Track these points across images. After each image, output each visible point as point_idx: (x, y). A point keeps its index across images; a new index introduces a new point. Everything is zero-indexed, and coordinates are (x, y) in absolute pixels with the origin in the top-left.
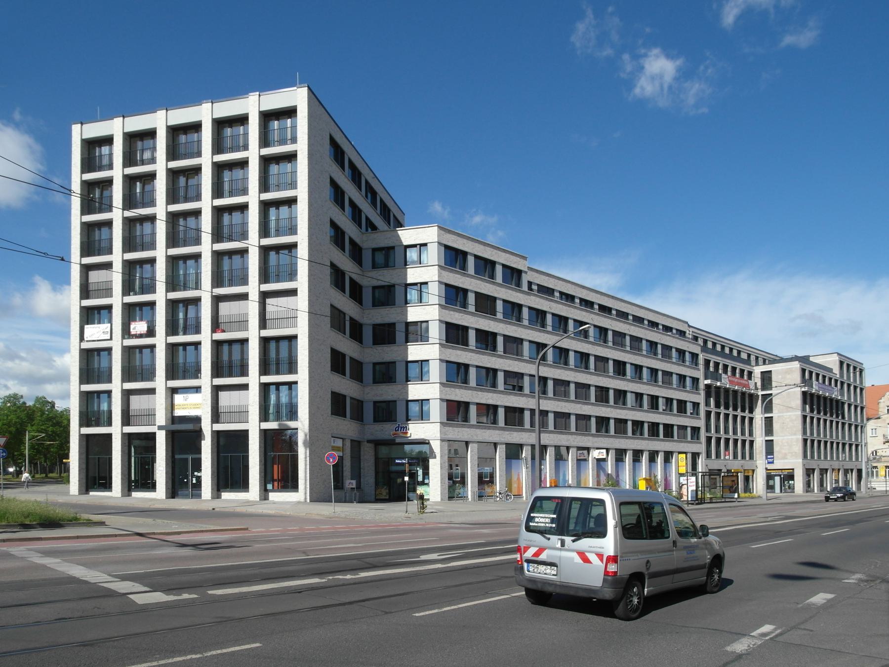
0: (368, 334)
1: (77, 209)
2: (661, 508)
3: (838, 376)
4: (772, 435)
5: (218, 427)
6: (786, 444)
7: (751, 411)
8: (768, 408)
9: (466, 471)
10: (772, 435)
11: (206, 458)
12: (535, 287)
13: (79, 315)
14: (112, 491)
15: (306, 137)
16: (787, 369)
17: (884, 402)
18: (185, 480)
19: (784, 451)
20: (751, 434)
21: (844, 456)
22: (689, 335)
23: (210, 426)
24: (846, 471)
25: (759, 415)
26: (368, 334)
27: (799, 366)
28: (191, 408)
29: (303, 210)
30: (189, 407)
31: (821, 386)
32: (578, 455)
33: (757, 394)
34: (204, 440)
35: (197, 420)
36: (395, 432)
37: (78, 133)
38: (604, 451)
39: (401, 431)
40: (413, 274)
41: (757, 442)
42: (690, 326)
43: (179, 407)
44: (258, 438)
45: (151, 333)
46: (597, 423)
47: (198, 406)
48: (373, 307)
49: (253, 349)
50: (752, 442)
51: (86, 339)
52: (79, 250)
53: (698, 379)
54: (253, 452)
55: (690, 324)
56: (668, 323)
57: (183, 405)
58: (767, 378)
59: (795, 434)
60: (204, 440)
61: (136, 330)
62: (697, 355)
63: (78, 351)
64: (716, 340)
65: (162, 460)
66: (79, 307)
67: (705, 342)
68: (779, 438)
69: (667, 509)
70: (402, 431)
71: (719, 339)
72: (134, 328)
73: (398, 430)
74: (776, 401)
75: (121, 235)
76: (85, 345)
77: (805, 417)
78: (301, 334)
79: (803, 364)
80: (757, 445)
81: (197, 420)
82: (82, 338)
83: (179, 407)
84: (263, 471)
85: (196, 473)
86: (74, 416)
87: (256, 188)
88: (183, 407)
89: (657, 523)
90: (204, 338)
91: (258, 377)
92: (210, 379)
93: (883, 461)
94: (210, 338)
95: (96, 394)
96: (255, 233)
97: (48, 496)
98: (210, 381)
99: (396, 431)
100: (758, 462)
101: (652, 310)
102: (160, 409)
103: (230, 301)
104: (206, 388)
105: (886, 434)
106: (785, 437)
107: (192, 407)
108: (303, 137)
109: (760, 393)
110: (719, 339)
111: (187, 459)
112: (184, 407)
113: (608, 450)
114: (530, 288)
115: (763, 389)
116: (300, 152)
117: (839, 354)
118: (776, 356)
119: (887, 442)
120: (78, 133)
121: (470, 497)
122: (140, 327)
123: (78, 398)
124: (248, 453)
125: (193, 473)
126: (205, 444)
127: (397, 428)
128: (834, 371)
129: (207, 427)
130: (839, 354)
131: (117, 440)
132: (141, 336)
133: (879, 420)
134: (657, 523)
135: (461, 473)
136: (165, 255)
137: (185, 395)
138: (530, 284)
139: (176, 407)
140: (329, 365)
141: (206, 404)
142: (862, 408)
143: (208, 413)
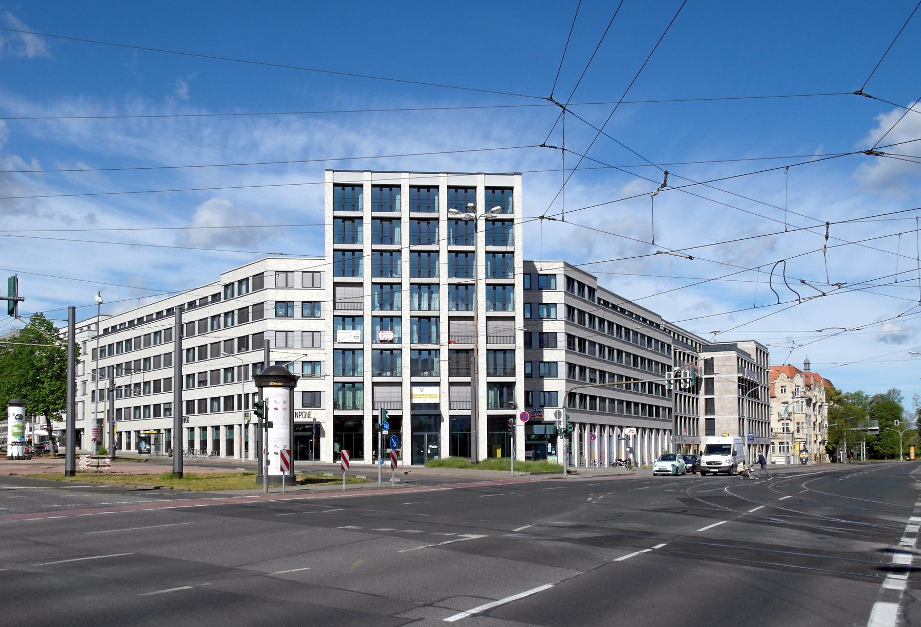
1: (330, 239)
3: (755, 361)
4: (713, 414)
5: (453, 413)
6: (725, 423)
7: (697, 394)
8: (710, 388)
10: (713, 414)
12: (602, 302)
14: (364, 460)
16: (727, 357)
17: (778, 382)
18: (422, 451)
19: (723, 429)
20: (697, 414)
25: (702, 396)
31: (749, 372)
33: (701, 377)
35: (437, 406)
37: (895, 421)
38: (635, 429)
41: (701, 420)
42: (662, 320)
46: (634, 406)
50: (698, 419)
51: (338, 341)
53: (671, 366)
56: (616, 302)
58: (709, 364)
59: (733, 414)
62: (671, 346)
64: (680, 332)
68: (719, 417)
69: (884, 463)
71: (678, 329)
74: (716, 385)
76: (337, 346)
77: (739, 399)
80: (701, 422)
81: (437, 406)
82: (335, 339)
85: (430, 446)
93: (778, 437)
100: (701, 438)
105: (780, 412)
106: (725, 417)
109: (704, 377)
110: (678, 329)
111: (423, 437)
112: (420, 397)
113: (637, 429)
114: (599, 303)
115: (705, 374)
117: (756, 342)
118: (705, 340)
119: (781, 420)
120: (895, 421)
121: (587, 464)
125: (428, 446)
128: (752, 357)
129: (445, 412)
130: (756, 342)
133: (775, 399)
138: (599, 299)
142: (768, 389)
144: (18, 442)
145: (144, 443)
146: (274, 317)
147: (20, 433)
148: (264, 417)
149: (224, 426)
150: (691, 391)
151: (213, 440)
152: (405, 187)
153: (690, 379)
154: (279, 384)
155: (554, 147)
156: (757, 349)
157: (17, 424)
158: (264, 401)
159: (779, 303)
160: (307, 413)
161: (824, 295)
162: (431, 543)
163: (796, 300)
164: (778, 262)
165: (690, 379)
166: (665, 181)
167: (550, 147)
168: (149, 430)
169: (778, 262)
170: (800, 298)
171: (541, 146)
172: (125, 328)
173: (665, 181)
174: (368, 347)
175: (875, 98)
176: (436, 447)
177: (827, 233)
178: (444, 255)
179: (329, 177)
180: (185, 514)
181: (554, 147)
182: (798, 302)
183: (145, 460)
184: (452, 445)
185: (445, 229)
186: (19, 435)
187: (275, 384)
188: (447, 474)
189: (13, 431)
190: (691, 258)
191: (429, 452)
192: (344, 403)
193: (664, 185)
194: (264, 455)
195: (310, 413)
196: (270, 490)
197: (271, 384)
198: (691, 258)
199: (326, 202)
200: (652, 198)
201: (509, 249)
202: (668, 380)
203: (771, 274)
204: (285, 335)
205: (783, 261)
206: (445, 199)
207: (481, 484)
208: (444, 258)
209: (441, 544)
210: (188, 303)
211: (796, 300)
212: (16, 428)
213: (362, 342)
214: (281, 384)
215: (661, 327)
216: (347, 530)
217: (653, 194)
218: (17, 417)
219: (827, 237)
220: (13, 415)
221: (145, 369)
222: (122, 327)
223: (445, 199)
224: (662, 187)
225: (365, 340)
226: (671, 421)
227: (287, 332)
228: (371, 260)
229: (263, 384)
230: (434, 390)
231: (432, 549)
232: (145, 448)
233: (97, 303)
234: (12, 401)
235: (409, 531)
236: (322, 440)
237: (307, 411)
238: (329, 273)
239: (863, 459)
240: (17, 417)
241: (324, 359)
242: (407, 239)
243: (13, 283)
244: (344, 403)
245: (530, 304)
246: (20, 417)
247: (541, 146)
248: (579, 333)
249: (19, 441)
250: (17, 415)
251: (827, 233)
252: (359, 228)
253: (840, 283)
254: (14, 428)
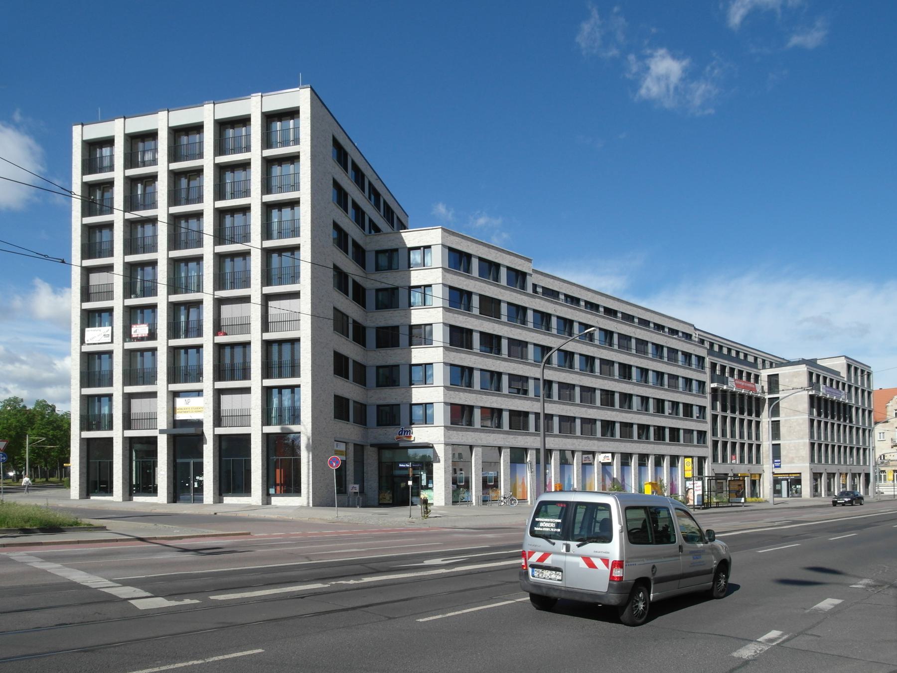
0: (371, 337)
1: (78, 211)
2: (667, 512)
3: (846, 379)
4: (779, 439)
5: (220, 431)
7: (758, 415)
8: (775, 411)
10: (779, 439)
11: (208, 462)
12: (539, 290)
13: (79, 318)
14: (113, 496)
15: (309, 138)
16: (794, 372)
17: (892, 406)
18: (187, 485)
19: (791, 455)
20: (758, 438)
21: (852, 460)
22: (695, 338)
23: (212, 429)
24: (854, 476)
25: (766, 419)
26: (371, 337)
28: (192, 412)
29: (306, 212)
30: (191, 410)
32: (584, 459)
33: (764, 398)
34: (206, 444)
35: (199, 424)
36: (398, 435)
37: (79, 134)
38: (610, 455)
39: (404, 434)
40: (417, 277)
41: (764, 446)
42: (696, 329)
43: (181, 411)
44: (261, 442)
45: (152, 336)
46: (602, 427)
47: (199, 410)
48: (376, 309)
49: (256, 352)
50: (758, 446)
51: (86, 342)
52: (80, 252)
53: (704, 383)
54: (256, 456)
55: (696, 327)
56: (674, 326)
57: (184, 409)
58: (773, 381)
59: (802, 438)
60: (206, 444)
61: (137, 333)
62: (703, 358)
63: (79, 355)
64: (722, 343)
65: (163, 464)
66: (79, 310)
67: (712, 345)
68: (786, 442)
70: (406, 435)
71: (725, 342)
72: (136, 331)
73: (402, 434)
74: (783, 405)
75: (122, 237)
76: (86, 349)
77: (812, 421)
78: (304, 337)
80: (764, 449)
81: (199, 424)
82: (82, 341)
83: (181, 411)
84: (266, 475)
86: (75, 420)
87: (258, 189)
88: (185, 411)
89: (663, 527)
90: (206, 341)
91: (260, 381)
92: (212, 382)
93: (891, 465)
94: (212, 341)
95: (96, 398)
96: (257, 235)
97: (49, 500)
98: (212, 385)
99: (399, 435)
100: (764, 466)
101: (658, 313)
102: (161, 413)
103: (232, 304)
104: (208, 392)
105: (894, 438)
106: (792, 441)
107: (194, 410)
108: (306, 139)
109: (767, 396)
110: (725, 342)
111: (188, 464)
112: (185, 411)
113: (613, 454)
114: (535, 291)
115: (770, 393)
116: (303, 154)
117: (846, 357)
118: (783, 359)
119: (895, 446)
120: (79, 134)
121: (474, 501)
122: (141, 330)
123: (79, 402)
124: (251, 457)
125: (194, 477)
126: (207, 448)
127: (401, 432)
128: (841, 375)
129: (208, 431)
130: (846, 357)
131: (118, 443)
132: (142, 339)
133: (887, 424)
134: (663, 527)
135: (465, 477)
136: (166, 257)
137: (187, 399)
138: (535, 286)
139: (177, 411)
140: (332, 368)
141: (208, 407)
142: (870, 412)
143: (210, 416)
150: (738, 407)
156: (849, 366)
215: (693, 338)
226: (538, 435)
248: (462, 321)
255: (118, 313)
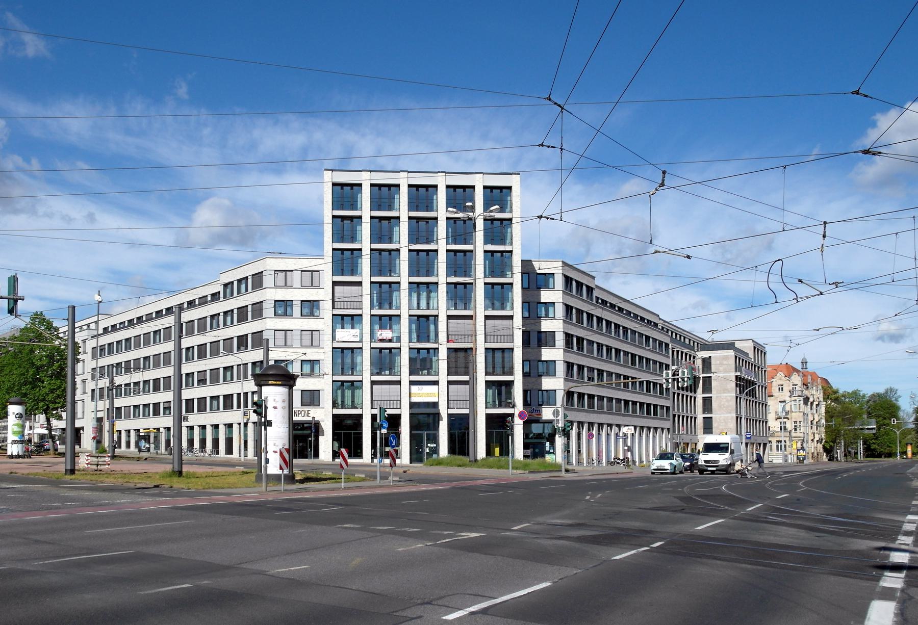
1: (329, 238)
3: (753, 360)
4: (711, 412)
5: (452, 411)
6: (723, 421)
7: (695, 392)
8: (708, 387)
9: (189, 431)
10: (711, 412)
12: (600, 301)
14: (363, 459)
16: (724, 356)
17: (776, 381)
18: (420, 450)
19: (721, 427)
20: (695, 413)
25: (700, 395)
27: (733, 354)
31: (747, 371)
33: (699, 376)
35: (435, 405)
37: (892, 419)
38: (633, 428)
41: (698, 419)
42: (660, 319)
46: (632, 404)
50: (695, 418)
51: (337, 340)
53: (669, 365)
56: (614, 301)
58: (707, 363)
59: (730, 413)
62: (668, 345)
64: (677, 331)
68: (717, 415)
69: (881, 461)
71: (676, 328)
74: (714, 384)
76: (336, 345)
77: (737, 397)
79: (736, 353)
80: (698, 421)
81: (435, 405)
82: (334, 338)
85: (429, 445)
93: (776, 435)
100: (699, 436)
105: (777, 411)
106: (722, 415)
109: (702, 375)
110: (676, 328)
111: (421, 435)
112: (419, 395)
113: (635, 427)
114: (597, 302)
115: (703, 372)
117: (753, 341)
118: (702, 339)
119: (778, 418)
120: (892, 419)
121: (585, 462)
125: (427, 445)
128: (750, 356)
129: (444, 411)
130: (753, 341)
133: (772, 398)
138: (597, 298)
142: (766, 388)
144: (18, 441)
145: (144, 442)
146: (273, 316)
147: (20, 431)
148: (263, 416)
149: (224, 424)
151: (212, 439)
152: (404, 186)
153: (688, 378)
154: (278, 383)
155: (552, 147)
157: (17, 422)
158: (263, 400)
159: (776, 302)
160: (306, 412)
161: (821, 294)
162: (430, 541)
163: (793, 299)
164: (776, 261)
165: (688, 378)
166: (663, 181)
167: (549, 147)
168: (149, 429)
169: (776, 261)
170: (797, 297)
171: (539, 145)
172: (125, 327)
173: (663, 181)
174: (367, 346)
175: (872, 98)
176: (435, 445)
177: (825, 232)
178: (443, 254)
179: (328, 177)
180: (184, 512)
181: (552, 147)
182: (796, 301)
183: (144, 459)
184: (450, 443)
185: (443, 228)
186: (19, 434)
187: (274, 383)
188: (445, 472)
189: (13, 429)
190: (688, 257)
191: (428, 451)
192: (343, 402)
193: (662, 185)
194: (263, 454)
195: (309, 412)
196: (269, 489)
197: (270, 382)
198: (688, 257)
199: (325, 201)
200: (650, 197)
201: (508, 248)
202: (666, 379)
203: (769, 273)
204: (284, 334)
205: (781, 260)
206: (443, 198)
207: (479, 482)
208: (442, 257)
209: (440, 542)
210: (188, 302)
211: (793, 299)
212: (16, 427)
213: (361, 341)
214: (280, 383)
216: (346, 528)
217: (651, 193)
218: (17, 416)
219: (824, 236)
220: (13, 413)
221: (144, 368)
222: (122, 326)
223: (443, 198)
224: (660, 186)
225: (364, 339)
227: (286, 331)
228: (369, 259)
229: (262, 383)
230: (433, 389)
231: (430, 547)
232: (144, 447)
233: (97, 302)
234: (12, 400)
235: (408, 529)
236: (321, 439)
237: (306, 410)
238: (328, 272)
239: (860, 458)
240: (17, 416)
241: (323, 358)
242: (406, 239)
243: (13, 282)
244: (343, 402)
245: (529, 303)
246: (20, 416)
247: (539, 145)
249: (19, 440)
250: (17, 414)
251: (825, 232)
252: (358, 227)
253: (838, 283)
254: (14, 427)
255: (367, 320)
